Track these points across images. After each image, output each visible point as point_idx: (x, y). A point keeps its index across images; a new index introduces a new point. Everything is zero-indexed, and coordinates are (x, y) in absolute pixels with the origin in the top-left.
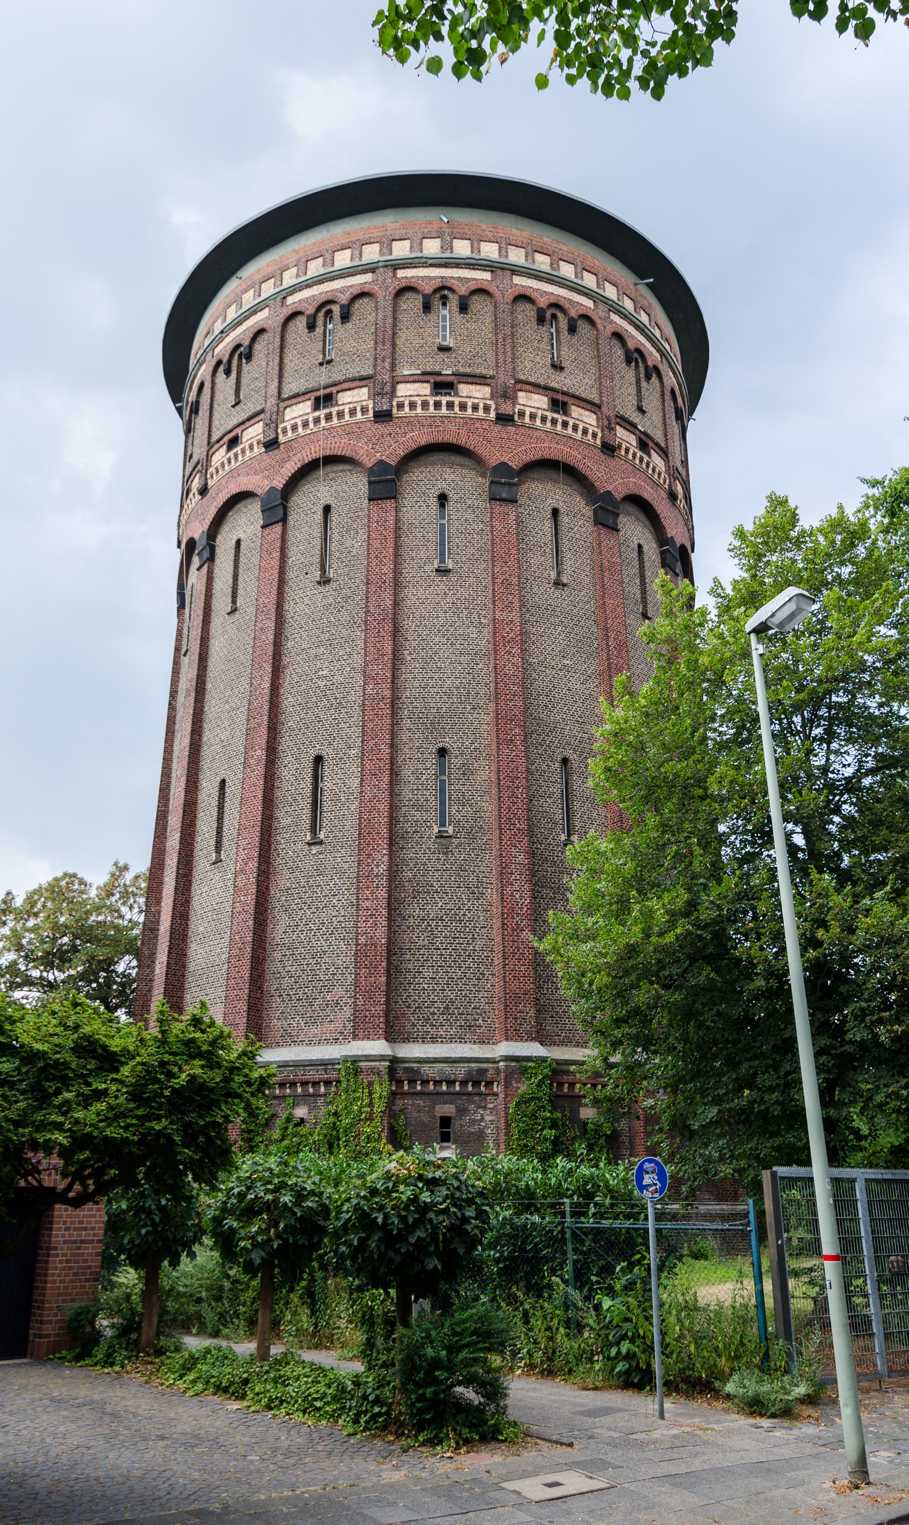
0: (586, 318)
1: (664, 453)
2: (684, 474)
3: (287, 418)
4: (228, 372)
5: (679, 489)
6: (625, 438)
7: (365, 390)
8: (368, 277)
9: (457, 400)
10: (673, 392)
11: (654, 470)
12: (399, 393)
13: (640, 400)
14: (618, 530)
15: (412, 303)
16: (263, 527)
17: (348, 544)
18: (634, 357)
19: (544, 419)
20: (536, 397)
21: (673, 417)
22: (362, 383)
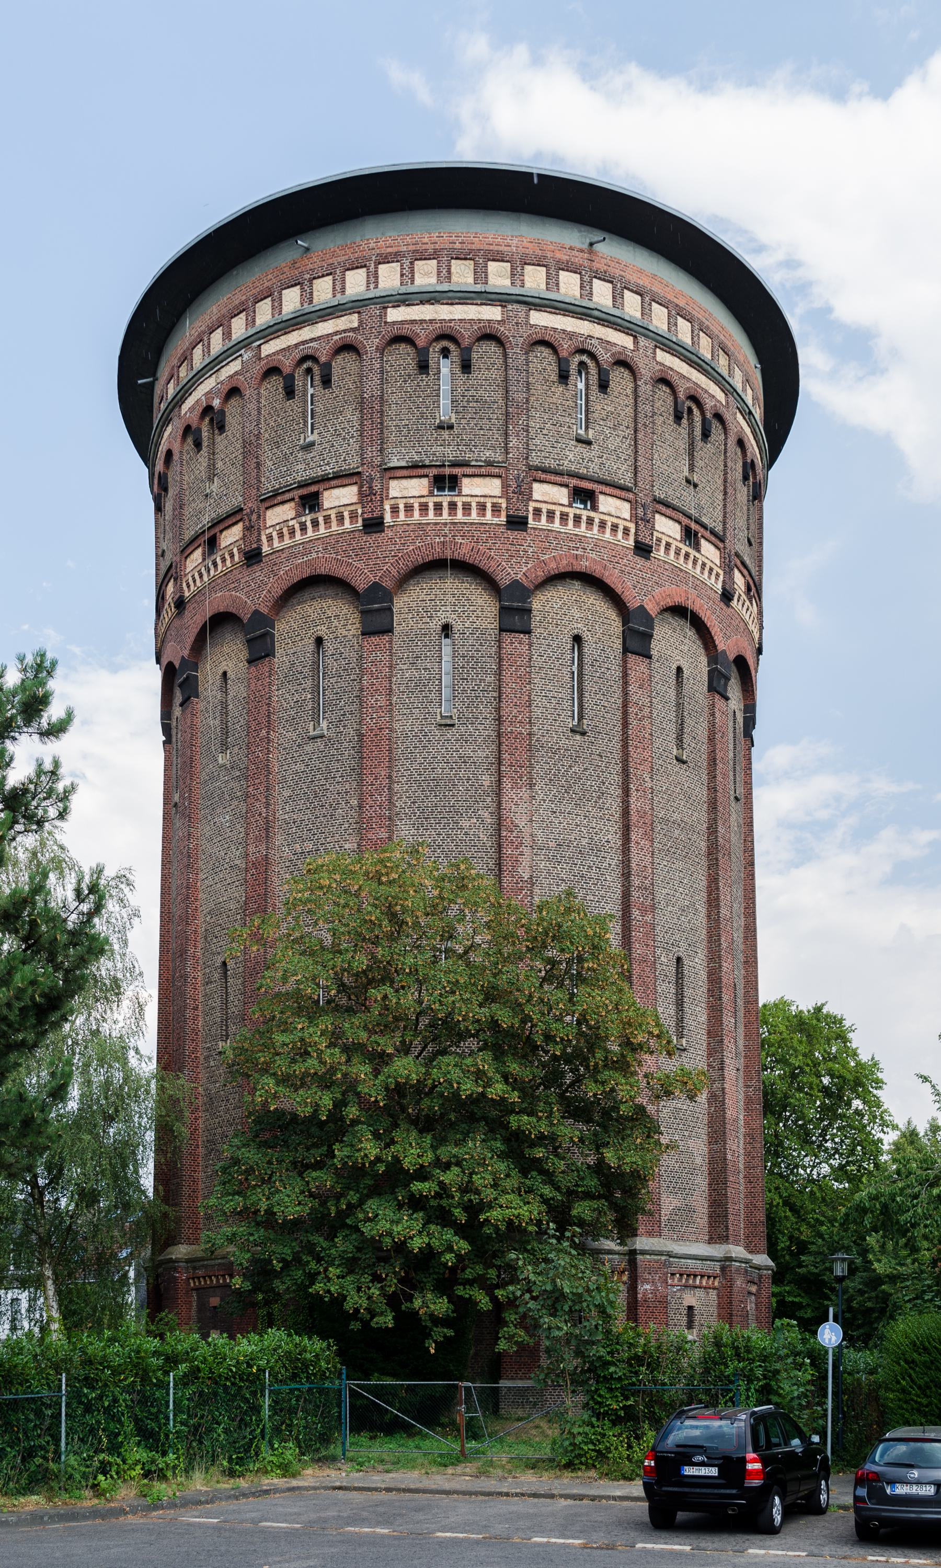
0: (622, 363)
1: (719, 539)
2: (760, 476)
3: (269, 524)
8: (353, 321)
9: (459, 501)
10: (741, 443)
11: (703, 568)
12: (392, 493)
14: (649, 657)
18: (687, 406)
19: (564, 517)
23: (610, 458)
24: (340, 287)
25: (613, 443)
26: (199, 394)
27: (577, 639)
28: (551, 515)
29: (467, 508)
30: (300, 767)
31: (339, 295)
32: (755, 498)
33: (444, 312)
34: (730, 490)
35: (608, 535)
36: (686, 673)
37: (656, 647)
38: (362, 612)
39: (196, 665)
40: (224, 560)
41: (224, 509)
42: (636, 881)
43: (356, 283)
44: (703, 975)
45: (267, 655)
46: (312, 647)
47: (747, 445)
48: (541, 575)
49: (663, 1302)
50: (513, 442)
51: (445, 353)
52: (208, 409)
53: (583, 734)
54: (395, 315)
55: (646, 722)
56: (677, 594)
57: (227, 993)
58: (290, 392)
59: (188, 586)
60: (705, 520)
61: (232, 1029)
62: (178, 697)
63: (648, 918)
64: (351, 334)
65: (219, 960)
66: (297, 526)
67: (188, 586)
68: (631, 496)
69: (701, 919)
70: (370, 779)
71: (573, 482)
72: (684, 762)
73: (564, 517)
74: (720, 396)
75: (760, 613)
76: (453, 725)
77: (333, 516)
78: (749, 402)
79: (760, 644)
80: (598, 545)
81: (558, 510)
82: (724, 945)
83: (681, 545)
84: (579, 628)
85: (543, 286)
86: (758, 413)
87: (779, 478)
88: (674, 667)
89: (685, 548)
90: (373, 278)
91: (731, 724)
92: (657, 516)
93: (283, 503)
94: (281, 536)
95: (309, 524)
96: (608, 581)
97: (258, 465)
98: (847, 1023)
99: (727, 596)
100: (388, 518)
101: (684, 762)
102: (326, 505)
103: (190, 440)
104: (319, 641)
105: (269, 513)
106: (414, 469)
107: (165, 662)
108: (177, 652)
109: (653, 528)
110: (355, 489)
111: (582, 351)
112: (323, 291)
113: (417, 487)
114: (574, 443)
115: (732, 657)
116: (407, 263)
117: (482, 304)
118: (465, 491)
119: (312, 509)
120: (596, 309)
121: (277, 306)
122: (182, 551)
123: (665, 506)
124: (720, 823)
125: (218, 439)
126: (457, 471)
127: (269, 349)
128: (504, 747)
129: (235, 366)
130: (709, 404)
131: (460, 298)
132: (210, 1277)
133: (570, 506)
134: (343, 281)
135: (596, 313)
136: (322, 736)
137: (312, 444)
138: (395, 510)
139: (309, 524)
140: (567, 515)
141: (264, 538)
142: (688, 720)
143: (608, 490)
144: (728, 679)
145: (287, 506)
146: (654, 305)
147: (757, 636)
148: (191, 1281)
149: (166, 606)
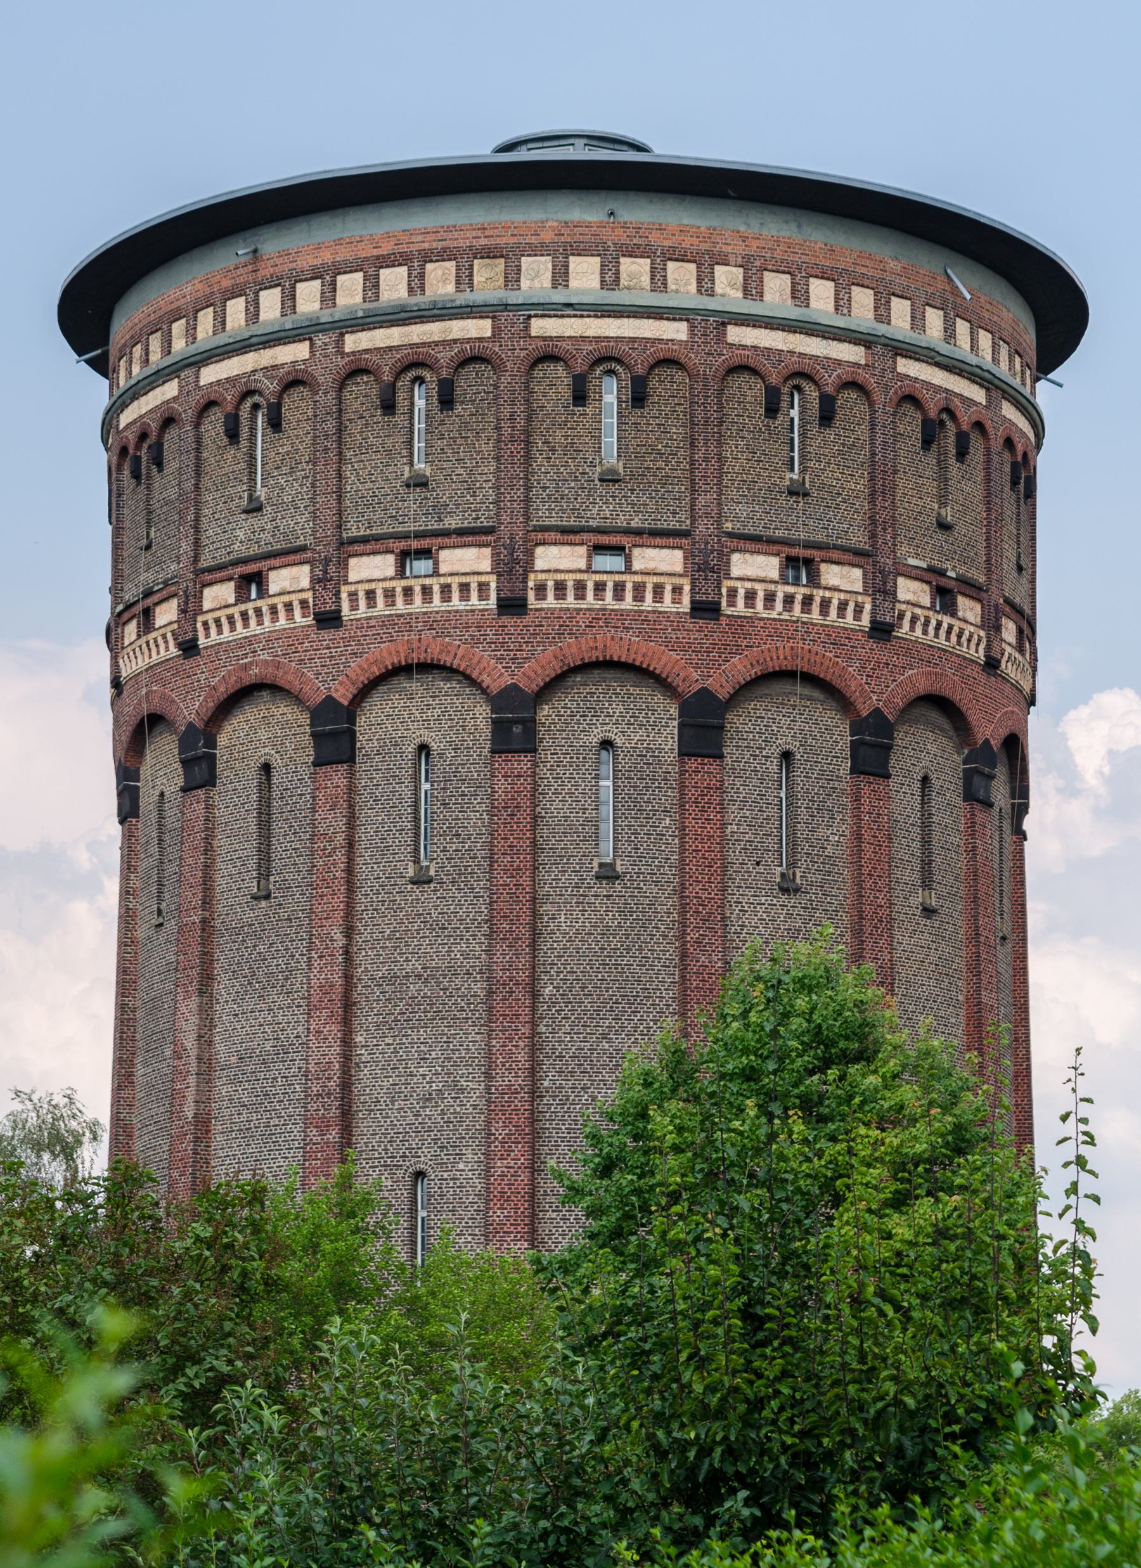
7: (857, 573)
12: (539, 564)
15: (362, 393)
16: (184, 790)
17: (820, 832)
20: (760, 559)
22: (856, 560)
36: (936, 783)
53: (267, 897)
80: (270, 639)
98: (1094, 1291)
114: (243, 516)
117: (164, 383)
120: (252, 336)
131: (149, 384)
135: (254, 340)
143: (276, 562)
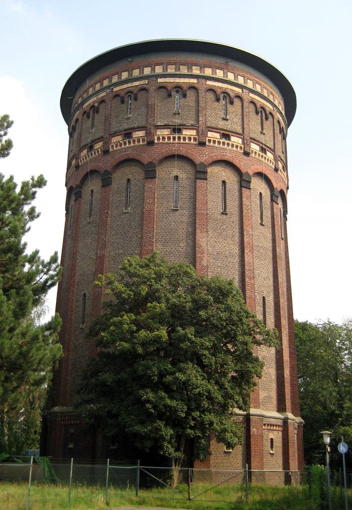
0: (238, 97)
1: (273, 151)
2: (285, 132)
3: (112, 142)
4: (88, 117)
5: (280, 165)
6: (255, 147)
10: (279, 122)
13: (262, 129)
14: (250, 189)
18: (260, 111)
19: (219, 143)
21: (278, 132)
23: (234, 124)
24: (142, 71)
25: (235, 120)
26: (90, 101)
27: (224, 182)
28: (214, 142)
29: (184, 139)
30: (119, 223)
31: (141, 75)
32: (284, 139)
33: (177, 80)
34: (276, 136)
35: (234, 148)
37: (252, 186)
38: (145, 171)
39: (82, 187)
40: (95, 153)
41: (97, 137)
42: (247, 268)
43: (147, 71)
44: (273, 304)
45: (109, 184)
46: (126, 182)
47: (281, 123)
48: (211, 161)
49: (262, 436)
50: (201, 119)
51: (177, 92)
52: (93, 106)
54: (160, 80)
55: (249, 211)
56: (259, 169)
57: (85, 305)
58: (123, 102)
59: (81, 161)
60: (268, 145)
61: (86, 319)
62: (73, 197)
63: (252, 281)
64: (145, 86)
65: (82, 293)
66: (123, 143)
67: (81, 161)
68: (242, 137)
69: (271, 282)
70: (146, 228)
71: (222, 132)
72: (263, 225)
73: (219, 143)
74: (271, 107)
75: (287, 176)
76: (178, 210)
77: (136, 140)
78: (281, 110)
79: (288, 186)
81: (217, 140)
82: (280, 292)
83: (260, 153)
84: (224, 178)
85: (211, 73)
86: (283, 113)
87: (291, 131)
88: (259, 192)
89: (261, 154)
90: (153, 70)
91: (279, 212)
92: (251, 143)
93: (118, 135)
94: (117, 146)
95: (127, 142)
96: (235, 163)
97: (110, 124)
99: (276, 170)
100: (156, 141)
101: (263, 225)
102: (134, 136)
103: (85, 116)
104: (129, 180)
105: (113, 139)
106: (166, 127)
107: (69, 186)
108: (75, 183)
109: (250, 147)
110: (144, 132)
111: (224, 93)
112: (136, 73)
113: (166, 132)
115: (279, 190)
116: (165, 66)
118: (184, 133)
119: (128, 138)
121: (120, 77)
122: (79, 150)
123: (254, 140)
124: (277, 247)
125: (96, 115)
126: (180, 127)
127: (116, 89)
128: (197, 218)
129: (104, 94)
130: (267, 110)
132: (71, 420)
133: (221, 139)
134: (143, 70)
136: (128, 213)
137: (130, 118)
138: (159, 139)
139: (127, 142)
140: (220, 142)
141: (110, 146)
142: (264, 211)
143: (234, 134)
144: (278, 197)
145: (119, 137)
146: (248, 80)
147: (286, 183)
148: (62, 422)
149: (72, 168)
